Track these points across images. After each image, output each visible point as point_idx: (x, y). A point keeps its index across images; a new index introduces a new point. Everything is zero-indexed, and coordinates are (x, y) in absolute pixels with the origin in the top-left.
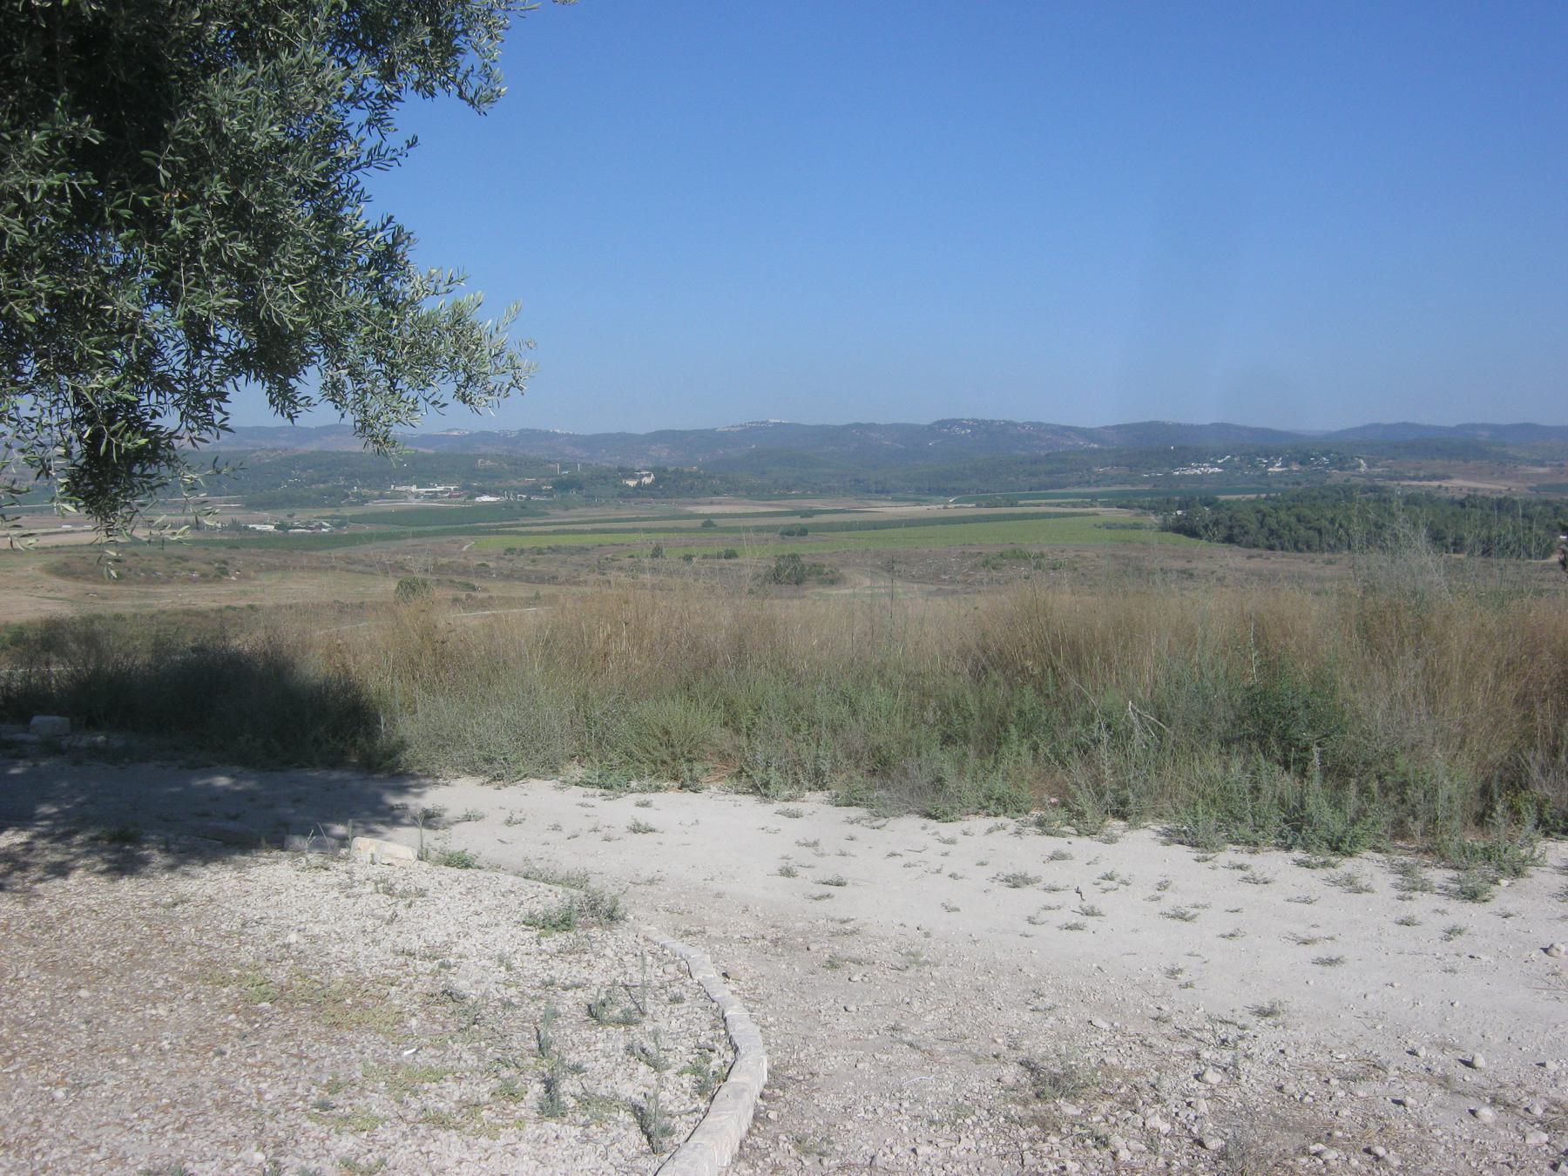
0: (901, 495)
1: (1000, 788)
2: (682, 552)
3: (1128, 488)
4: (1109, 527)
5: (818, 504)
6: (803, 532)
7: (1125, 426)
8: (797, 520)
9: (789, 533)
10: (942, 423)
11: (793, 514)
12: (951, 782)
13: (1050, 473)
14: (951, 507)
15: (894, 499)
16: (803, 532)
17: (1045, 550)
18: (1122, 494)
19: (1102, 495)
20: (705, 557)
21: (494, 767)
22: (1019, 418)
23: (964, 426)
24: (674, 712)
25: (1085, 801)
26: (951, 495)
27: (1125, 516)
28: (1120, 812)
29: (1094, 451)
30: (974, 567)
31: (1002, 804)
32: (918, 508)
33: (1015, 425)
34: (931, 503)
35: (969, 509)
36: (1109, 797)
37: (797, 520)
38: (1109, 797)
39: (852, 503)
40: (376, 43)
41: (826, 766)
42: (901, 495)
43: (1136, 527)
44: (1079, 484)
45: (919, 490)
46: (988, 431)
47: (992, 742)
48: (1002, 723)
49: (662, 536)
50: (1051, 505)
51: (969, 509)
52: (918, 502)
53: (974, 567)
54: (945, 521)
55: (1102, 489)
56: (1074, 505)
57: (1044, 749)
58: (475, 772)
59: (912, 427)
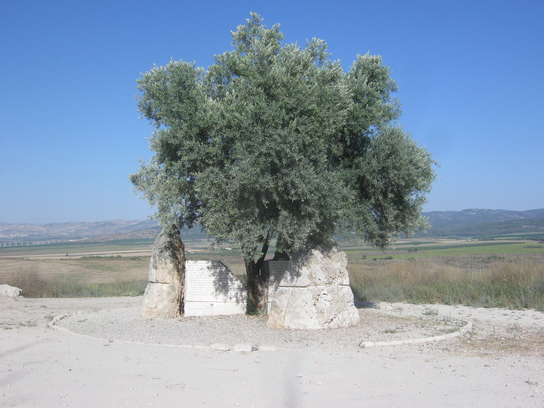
0: (451, 236)
1: (500, 302)
2: (374, 257)
3: (536, 233)
4: (529, 247)
5: (421, 240)
6: (416, 250)
7: (534, 210)
8: (413, 246)
9: (410, 250)
10: (466, 211)
11: (412, 243)
12: (490, 302)
13: (506, 228)
14: (469, 241)
15: (448, 238)
16: (416, 250)
17: (505, 256)
18: (534, 235)
19: (526, 236)
20: (381, 259)
21: (387, 299)
22: (493, 208)
23: (474, 212)
24: (426, 288)
25: (518, 304)
26: (470, 236)
27: (535, 243)
28: (526, 307)
29: (522, 220)
30: (478, 262)
31: (500, 306)
32: (459, 241)
33: (492, 211)
34: (462, 239)
35: (476, 241)
36: (523, 304)
37: (413, 246)
38: (523, 304)
39: (433, 240)
40: (359, 151)
41: (462, 299)
42: (451, 236)
43: (539, 247)
44: (517, 232)
45: (457, 235)
46: (481, 212)
47: (498, 295)
48: (499, 291)
49: (366, 252)
50: (506, 239)
51: (476, 241)
52: (457, 239)
53: (478, 262)
54: (467, 246)
55: (525, 233)
56: (515, 240)
57: (509, 297)
58: (385, 301)
59: (454, 212)
